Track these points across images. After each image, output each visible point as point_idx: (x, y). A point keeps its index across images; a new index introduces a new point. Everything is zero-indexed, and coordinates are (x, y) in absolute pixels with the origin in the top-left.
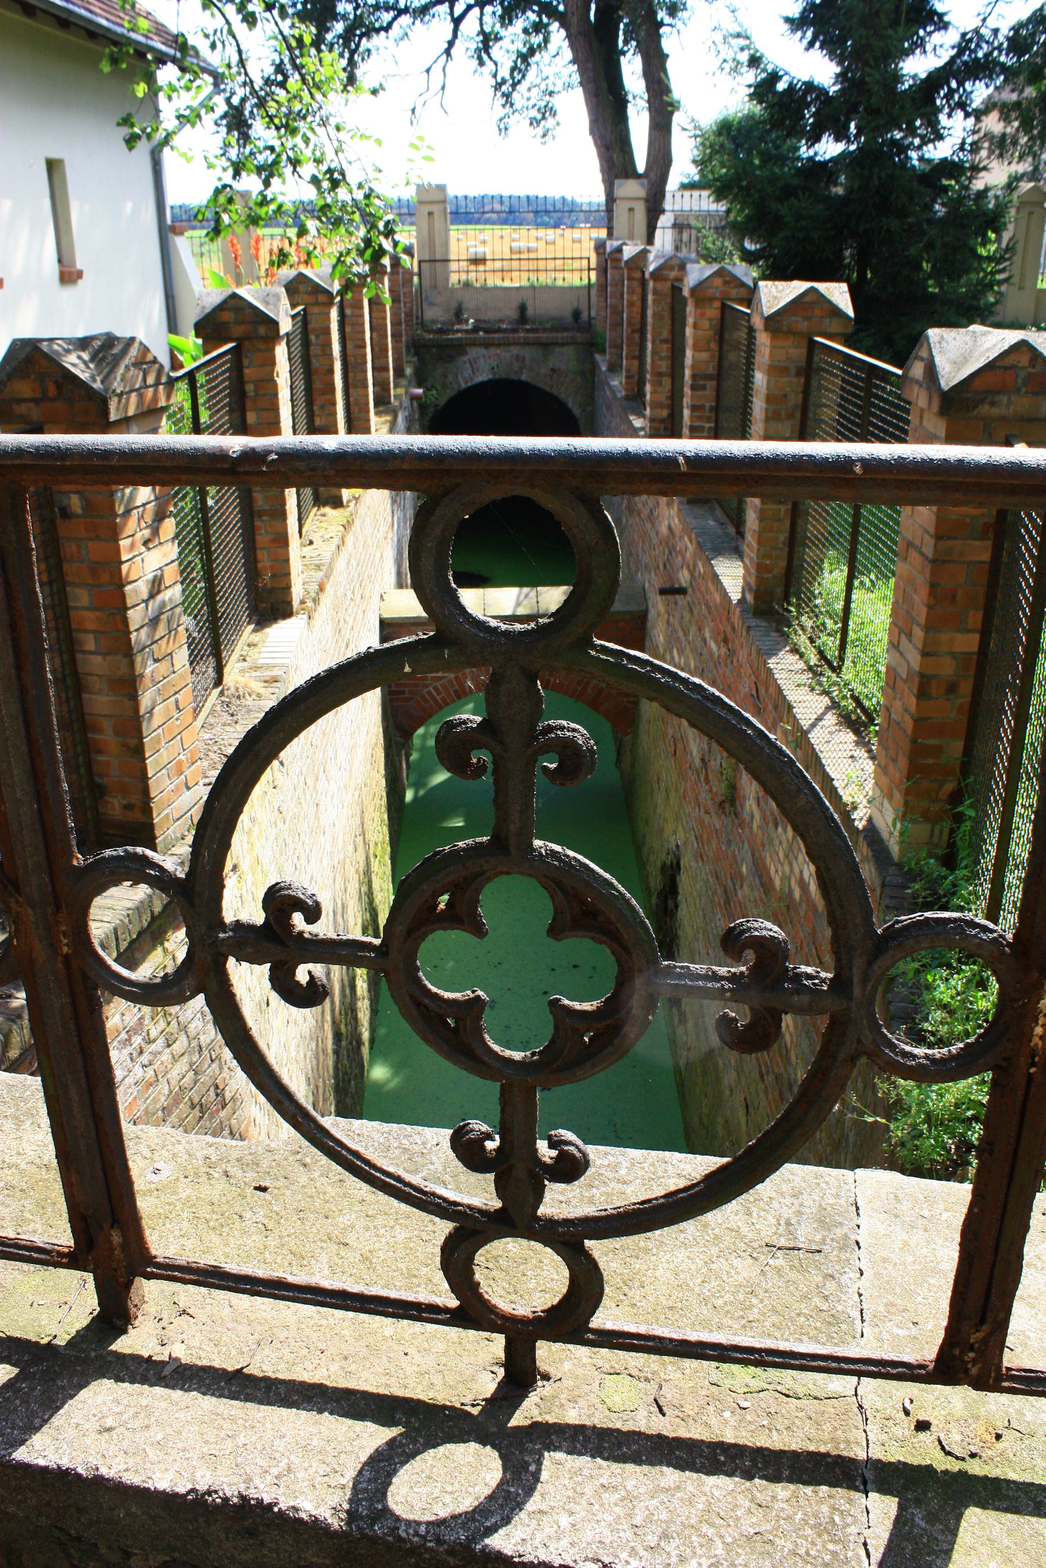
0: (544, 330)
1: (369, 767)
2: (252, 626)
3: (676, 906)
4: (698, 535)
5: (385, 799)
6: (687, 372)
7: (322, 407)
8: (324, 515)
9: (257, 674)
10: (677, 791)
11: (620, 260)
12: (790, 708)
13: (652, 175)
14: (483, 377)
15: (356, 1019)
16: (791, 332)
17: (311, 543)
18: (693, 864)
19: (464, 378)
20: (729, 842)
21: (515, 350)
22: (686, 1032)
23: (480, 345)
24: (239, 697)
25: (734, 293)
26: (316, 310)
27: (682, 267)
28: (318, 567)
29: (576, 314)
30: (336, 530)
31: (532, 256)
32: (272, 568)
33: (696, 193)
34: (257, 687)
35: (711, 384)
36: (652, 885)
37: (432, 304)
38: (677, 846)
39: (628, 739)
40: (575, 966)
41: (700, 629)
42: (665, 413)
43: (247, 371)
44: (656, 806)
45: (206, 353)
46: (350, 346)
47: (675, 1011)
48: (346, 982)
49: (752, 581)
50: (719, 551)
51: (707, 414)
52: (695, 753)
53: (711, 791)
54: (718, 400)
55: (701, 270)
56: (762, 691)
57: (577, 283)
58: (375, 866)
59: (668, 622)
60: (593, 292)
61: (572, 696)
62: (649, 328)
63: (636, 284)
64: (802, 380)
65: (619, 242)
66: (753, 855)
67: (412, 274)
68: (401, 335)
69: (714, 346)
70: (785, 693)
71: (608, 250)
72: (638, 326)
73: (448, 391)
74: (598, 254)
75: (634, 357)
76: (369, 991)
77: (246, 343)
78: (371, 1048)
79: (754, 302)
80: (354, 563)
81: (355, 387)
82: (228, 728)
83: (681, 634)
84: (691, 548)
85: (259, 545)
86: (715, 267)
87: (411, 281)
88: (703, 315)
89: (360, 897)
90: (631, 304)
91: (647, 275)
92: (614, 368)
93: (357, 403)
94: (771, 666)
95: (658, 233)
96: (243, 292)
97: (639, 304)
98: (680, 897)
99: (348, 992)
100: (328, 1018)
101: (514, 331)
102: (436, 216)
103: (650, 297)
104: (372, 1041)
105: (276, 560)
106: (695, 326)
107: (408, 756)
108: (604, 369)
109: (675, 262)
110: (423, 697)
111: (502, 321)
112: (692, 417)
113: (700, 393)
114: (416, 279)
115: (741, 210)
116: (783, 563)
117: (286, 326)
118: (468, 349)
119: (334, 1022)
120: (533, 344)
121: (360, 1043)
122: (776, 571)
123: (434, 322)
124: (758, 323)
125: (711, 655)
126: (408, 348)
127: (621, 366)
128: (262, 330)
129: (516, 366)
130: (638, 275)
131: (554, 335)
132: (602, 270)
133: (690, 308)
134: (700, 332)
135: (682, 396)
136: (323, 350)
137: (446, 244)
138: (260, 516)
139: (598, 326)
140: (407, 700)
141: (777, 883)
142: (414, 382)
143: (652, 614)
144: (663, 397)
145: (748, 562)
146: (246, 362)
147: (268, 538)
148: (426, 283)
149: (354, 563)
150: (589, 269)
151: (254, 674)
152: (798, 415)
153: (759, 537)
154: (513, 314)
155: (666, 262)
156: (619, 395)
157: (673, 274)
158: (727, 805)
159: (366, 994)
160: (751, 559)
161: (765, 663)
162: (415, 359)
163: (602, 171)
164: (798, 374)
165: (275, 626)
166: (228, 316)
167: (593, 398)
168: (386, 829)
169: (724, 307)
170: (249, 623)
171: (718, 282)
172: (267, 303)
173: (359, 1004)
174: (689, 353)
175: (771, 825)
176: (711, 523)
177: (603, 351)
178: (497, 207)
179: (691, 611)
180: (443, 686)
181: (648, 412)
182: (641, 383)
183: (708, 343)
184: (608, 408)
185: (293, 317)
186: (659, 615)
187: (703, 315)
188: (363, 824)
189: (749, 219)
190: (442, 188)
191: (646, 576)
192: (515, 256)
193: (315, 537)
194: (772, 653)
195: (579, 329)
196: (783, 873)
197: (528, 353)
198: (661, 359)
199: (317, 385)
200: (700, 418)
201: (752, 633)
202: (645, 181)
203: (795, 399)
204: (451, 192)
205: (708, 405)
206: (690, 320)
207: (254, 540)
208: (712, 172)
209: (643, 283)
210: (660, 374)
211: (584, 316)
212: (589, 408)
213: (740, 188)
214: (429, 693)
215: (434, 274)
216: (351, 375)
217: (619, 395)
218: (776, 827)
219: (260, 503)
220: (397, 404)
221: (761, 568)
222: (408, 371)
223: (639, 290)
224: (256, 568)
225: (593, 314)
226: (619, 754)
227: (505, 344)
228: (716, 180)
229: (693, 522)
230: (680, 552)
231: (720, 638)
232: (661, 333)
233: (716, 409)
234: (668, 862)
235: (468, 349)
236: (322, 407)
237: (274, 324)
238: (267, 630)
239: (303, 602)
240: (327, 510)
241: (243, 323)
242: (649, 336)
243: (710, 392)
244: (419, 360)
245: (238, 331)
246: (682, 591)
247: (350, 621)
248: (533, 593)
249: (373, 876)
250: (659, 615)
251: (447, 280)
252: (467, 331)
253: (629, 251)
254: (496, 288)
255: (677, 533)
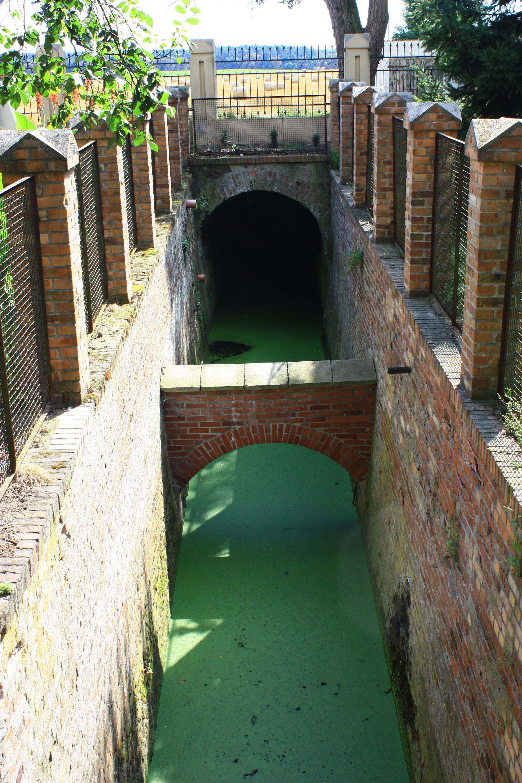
0: (291, 152)
1: (150, 514)
2: (44, 415)
3: (408, 635)
4: (420, 326)
5: (164, 538)
6: (408, 190)
7: (110, 223)
8: (112, 311)
9: (47, 460)
10: (405, 535)
11: (350, 97)
12: (510, 490)
13: (373, 29)
14: (243, 189)
15: (136, 739)
16: (500, 162)
17: (100, 336)
18: (421, 601)
19: (228, 190)
20: (454, 591)
21: (268, 168)
22: (419, 750)
23: (241, 164)
24: (29, 484)
25: (446, 125)
26: (105, 144)
27: (402, 103)
28: (105, 358)
29: (316, 139)
30: (120, 324)
31: (281, 93)
32: (63, 364)
33: (408, 43)
34: (45, 473)
35: (428, 200)
36: (386, 610)
37: (203, 132)
38: (407, 583)
39: (362, 484)
40: (323, 684)
41: (423, 404)
42: (389, 220)
43: (39, 200)
44: (388, 544)
45: (5, 186)
46: (135, 170)
47: (408, 727)
48: (128, 709)
49: (470, 371)
50: (438, 341)
51: (425, 224)
52: (421, 506)
53: (436, 542)
54: (434, 212)
55: (419, 108)
56: (482, 467)
57: (316, 114)
58: (155, 598)
59: (395, 393)
60: (329, 121)
61: (316, 449)
62: (375, 152)
63: (363, 116)
64: (511, 201)
65: (349, 83)
66: (477, 609)
67: (7, 297)
68: (178, 158)
69: (430, 169)
70: (506, 475)
71: (341, 89)
72: (365, 150)
73: (216, 200)
74: (332, 92)
75: (362, 174)
76: (149, 710)
77: (40, 176)
78: (150, 761)
79: (468, 136)
80: (137, 347)
81: (140, 202)
82: (17, 515)
83: (406, 404)
84: (414, 336)
85: (52, 344)
86: (430, 104)
87: (187, 115)
88: (421, 144)
89: (142, 629)
90: (360, 132)
91: (373, 110)
92: (346, 181)
93: (141, 215)
94: (490, 448)
95: (379, 74)
96: (36, 133)
97: (365, 132)
98: (410, 628)
99: (129, 717)
100: (110, 747)
101: (267, 153)
102: (205, 64)
103: (376, 128)
104: (151, 754)
105: (67, 358)
106: (414, 153)
107: (185, 496)
108: (338, 181)
109: (395, 99)
110: (196, 452)
111: (258, 145)
112: (412, 227)
113: (419, 207)
114: (190, 113)
115: (448, 56)
116: (497, 356)
117: (73, 161)
118: (232, 168)
119: (116, 749)
120: (282, 163)
121: (139, 760)
122: (490, 363)
123: (205, 146)
124: (471, 153)
125: (434, 427)
126: (184, 167)
127: (352, 180)
128: (52, 166)
129: (269, 180)
130: (365, 109)
131: (299, 156)
132: (336, 104)
133: (410, 138)
134: (418, 158)
135: (404, 209)
136: (111, 176)
137: (214, 86)
138: (53, 321)
139: (333, 148)
140: (184, 454)
141: (502, 640)
142: (189, 194)
143: (381, 384)
144: (387, 208)
145: (465, 354)
146: (39, 192)
147: (60, 339)
148: (198, 117)
149: (137, 347)
150: (326, 104)
151: (44, 460)
152: (508, 231)
153: (476, 334)
154: (267, 140)
155: (388, 99)
156: (351, 204)
157: (393, 109)
158: (452, 560)
159: (146, 714)
160: (469, 352)
161: (485, 446)
162: (190, 176)
163: (334, 28)
164: (507, 197)
165: (65, 413)
166: (23, 154)
167: (330, 205)
168: (165, 564)
169: (438, 136)
170: (42, 413)
171: (433, 116)
172: (57, 143)
173: (140, 725)
174: (409, 175)
175: (493, 586)
176: (431, 315)
177: (337, 168)
178: (253, 54)
179: (415, 387)
180: (212, 442)
181: (375, 219)
182: (369, 195)
183: (425, 166)
184: (342, 213)
185: (81, 153)
186: (387, 385)
187: (421, 144)
188: (144, 565)
189: (454, 64)
190: (210, 43)
191: (376, 352)
192: (268, 94)
193: (104, 331)
194: (490, 436)
195: (317, 152)
196: (507, 633)
197: (278, 170)
198: (385, 177)
199: (106, 204)
200: (419, 228)
201: (472, 417)
202: (369, 34)
203: (506, 218)
204: (218, 44)
205: (425, 217)
206: (410, 148)
207: (47, 341)
208: (423, 27)
209: (369, 115)
210: (384, 190)
211: (322, 141)
212: (327, 212)
213: (447, 39)
214: (201, 448)
215: (204, 109)
216: (136, 193)
217: (351, 204)
218: (499, 590)
219: (53, 310)
220: (175, 213)
221: (477, 360)
222: (185, 186)
223: (365, 121)
224: (49, 365)
225: (329, 139)
226: (355, 494)
227: (260, 164)
228: (427, 33)
229: (416, 315)
230: (405, 336)
231: (442, 414)
232: (385, 156)
233: (433, 220)
234: (399, 595)
235: (232, 168)
236: (110, 223)
237: (64, 160)
238: (58, 418)
239: (90, 391)
240: (115, 306)
241: (36, 160)
242: (375, 159)
243: (427, 206)
244: (193, 177)
245: (32, 166)
246: (407, 370)
247: (134, 397)
248: (284, 368)
249: (154, 608)
250: (387, 385)
251: (215, 113)
252: (230, 154)
253: (357, 91)
254: (253, 119)
255: (401, 320)
